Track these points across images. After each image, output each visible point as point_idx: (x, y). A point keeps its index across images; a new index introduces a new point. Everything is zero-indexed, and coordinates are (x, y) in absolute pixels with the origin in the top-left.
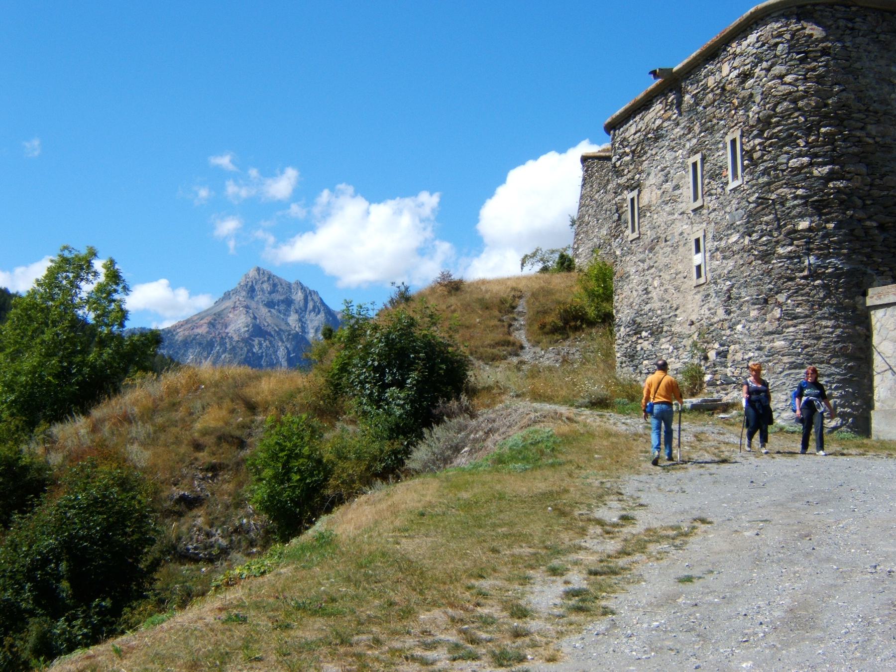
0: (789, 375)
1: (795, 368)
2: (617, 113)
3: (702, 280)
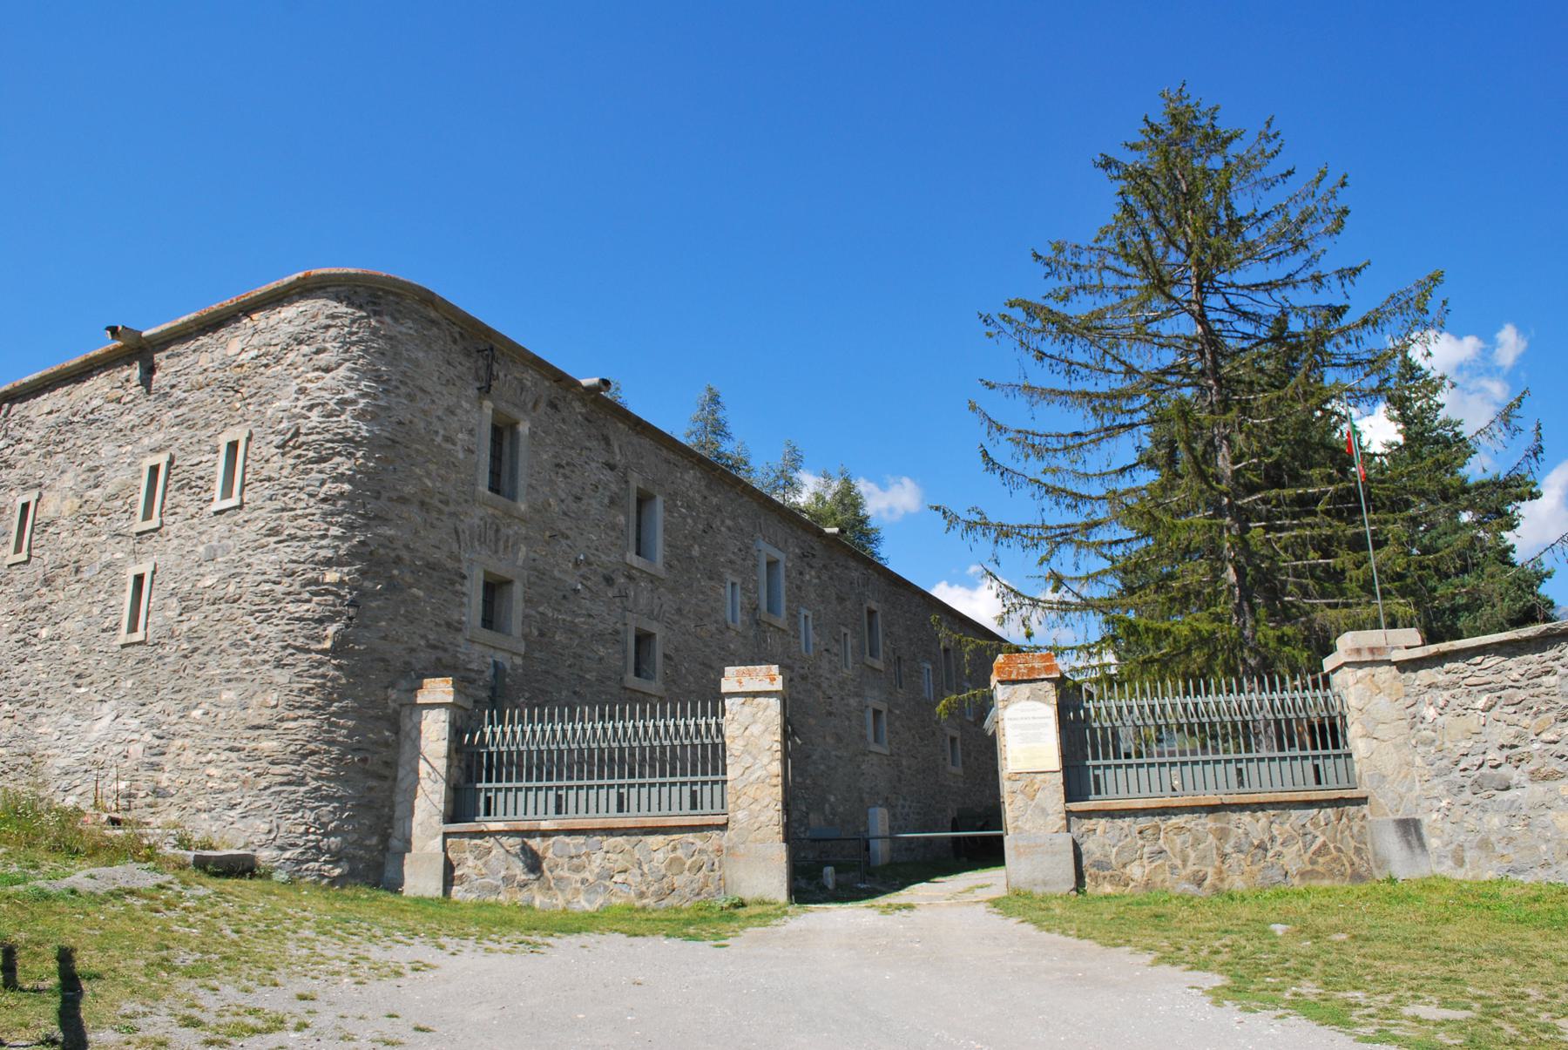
0: (279, 793)
1: (289, 783)
2: (26, 380)
3: (138, 636)
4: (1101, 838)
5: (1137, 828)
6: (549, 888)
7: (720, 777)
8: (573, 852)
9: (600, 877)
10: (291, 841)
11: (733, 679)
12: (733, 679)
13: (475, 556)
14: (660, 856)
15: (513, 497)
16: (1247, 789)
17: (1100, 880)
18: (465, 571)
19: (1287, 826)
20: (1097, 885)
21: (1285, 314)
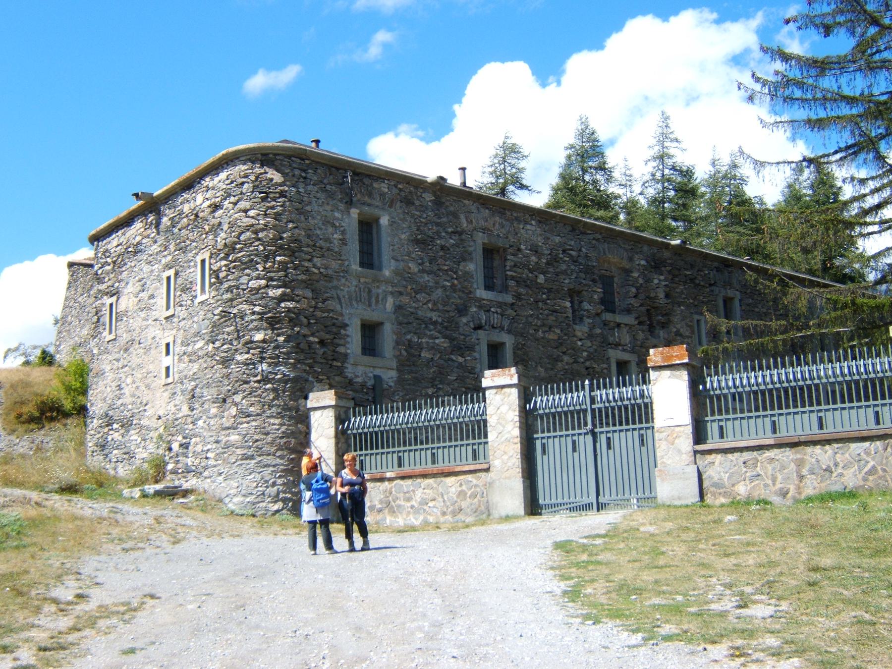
0: (241, 465)
1: (247, 459)
2: (102, 227)
4: (718, 468)
5: (742, 460)
6: (394, 512)
7: (483, 440)
8: (405, 490)
9: (421, 503)
10: (250, 491)
11: (490, 378)
12: (490, 378)
13: (352, 311)
14: (453, 490)
15: (380, 269)
16: (825, 431)
17: (717, 496)
18: (347, 321)
19: (847, 455)
20: (716, 498)
21: (568, 189)
